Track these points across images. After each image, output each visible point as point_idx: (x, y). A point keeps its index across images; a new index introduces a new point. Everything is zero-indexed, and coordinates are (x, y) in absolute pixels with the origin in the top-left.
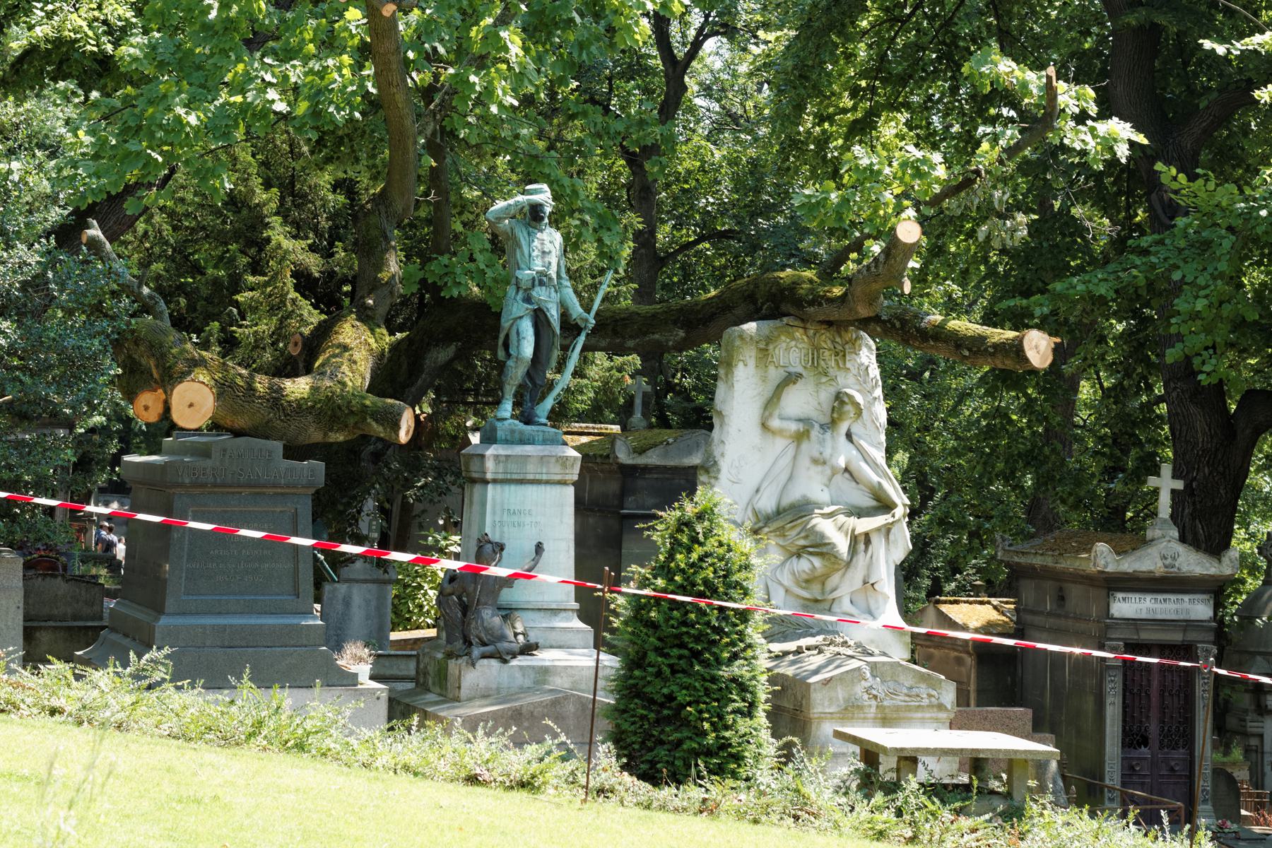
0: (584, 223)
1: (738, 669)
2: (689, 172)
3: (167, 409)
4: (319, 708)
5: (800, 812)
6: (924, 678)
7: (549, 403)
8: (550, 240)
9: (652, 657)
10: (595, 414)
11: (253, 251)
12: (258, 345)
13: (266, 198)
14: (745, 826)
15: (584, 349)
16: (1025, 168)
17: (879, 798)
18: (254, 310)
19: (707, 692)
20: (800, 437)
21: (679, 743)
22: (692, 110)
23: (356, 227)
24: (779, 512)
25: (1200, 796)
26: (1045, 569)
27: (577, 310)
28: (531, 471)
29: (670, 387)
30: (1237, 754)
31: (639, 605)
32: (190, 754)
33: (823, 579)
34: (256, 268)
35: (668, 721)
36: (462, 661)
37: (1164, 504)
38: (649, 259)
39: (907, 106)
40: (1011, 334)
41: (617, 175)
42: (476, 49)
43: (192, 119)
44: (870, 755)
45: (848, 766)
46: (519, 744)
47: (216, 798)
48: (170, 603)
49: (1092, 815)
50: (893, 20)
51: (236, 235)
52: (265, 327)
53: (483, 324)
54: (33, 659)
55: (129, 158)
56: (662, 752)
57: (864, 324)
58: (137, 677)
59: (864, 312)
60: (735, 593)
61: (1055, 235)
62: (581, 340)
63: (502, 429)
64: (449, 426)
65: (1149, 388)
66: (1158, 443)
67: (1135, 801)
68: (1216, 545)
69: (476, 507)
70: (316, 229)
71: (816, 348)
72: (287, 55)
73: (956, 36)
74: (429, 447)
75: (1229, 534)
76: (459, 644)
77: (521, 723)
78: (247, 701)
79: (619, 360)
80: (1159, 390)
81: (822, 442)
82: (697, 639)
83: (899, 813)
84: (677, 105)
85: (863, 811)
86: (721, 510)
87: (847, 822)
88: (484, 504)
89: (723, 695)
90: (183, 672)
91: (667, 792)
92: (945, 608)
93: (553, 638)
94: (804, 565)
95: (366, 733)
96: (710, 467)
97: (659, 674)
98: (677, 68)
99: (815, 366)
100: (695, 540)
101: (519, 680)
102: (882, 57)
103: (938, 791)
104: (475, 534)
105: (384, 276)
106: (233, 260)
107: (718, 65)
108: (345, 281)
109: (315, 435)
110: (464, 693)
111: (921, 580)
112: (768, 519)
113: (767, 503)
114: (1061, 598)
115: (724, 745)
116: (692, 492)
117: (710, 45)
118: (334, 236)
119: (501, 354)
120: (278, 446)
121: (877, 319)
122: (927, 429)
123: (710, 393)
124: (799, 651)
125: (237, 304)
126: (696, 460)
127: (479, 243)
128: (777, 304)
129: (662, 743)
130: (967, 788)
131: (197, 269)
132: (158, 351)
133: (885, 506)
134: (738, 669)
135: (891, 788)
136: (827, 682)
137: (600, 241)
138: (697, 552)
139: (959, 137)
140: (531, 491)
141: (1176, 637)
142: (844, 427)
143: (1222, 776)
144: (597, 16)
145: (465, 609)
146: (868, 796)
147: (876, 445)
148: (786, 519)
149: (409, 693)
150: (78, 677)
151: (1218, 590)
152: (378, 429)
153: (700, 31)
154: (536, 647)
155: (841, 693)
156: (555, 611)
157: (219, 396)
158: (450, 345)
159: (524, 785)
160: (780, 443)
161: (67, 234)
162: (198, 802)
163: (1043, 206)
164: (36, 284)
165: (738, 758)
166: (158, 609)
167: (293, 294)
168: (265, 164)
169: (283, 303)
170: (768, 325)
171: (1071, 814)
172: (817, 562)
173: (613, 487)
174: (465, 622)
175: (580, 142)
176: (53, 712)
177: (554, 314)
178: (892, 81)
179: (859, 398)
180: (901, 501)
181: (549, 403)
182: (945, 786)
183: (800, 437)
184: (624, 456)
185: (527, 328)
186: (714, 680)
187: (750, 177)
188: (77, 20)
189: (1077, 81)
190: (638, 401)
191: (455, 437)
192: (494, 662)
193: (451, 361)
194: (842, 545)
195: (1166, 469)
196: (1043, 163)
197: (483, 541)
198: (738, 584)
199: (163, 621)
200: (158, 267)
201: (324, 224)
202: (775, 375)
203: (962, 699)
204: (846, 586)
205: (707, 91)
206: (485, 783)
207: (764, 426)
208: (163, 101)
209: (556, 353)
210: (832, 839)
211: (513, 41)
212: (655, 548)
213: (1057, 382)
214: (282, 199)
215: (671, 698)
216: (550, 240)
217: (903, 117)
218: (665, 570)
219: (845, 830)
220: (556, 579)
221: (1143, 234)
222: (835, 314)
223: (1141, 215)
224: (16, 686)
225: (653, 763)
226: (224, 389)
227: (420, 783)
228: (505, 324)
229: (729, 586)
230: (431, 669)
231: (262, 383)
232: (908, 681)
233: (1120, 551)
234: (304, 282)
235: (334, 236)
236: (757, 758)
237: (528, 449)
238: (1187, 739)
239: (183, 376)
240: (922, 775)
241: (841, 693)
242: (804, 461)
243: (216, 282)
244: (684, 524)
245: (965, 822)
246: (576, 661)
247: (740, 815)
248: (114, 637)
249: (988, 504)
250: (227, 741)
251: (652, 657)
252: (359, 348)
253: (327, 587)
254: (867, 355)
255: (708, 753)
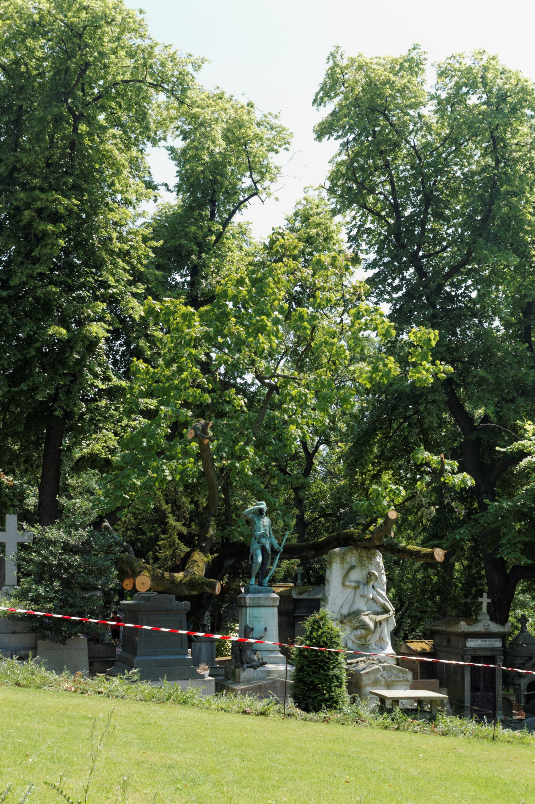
0: (278, 514)
1: (336, 671)
2: (315, 493)
3: (134, 585)
4: (191, 688)
5: (358, 719)
6: (401, 671)
7: (268, 578)
8: (266, 521)
9: (306, 668)
10: (284, 580)
11: (163, 526)
12: (166, 559)
13: (165, 507)
14: (340, 726)
15: (280, 559)
16: (434, 489)
17: (385, 715)
18: (164, 547)
19: (325, 679)
20: (356, 588)
21: (316, 697)
22: (316, 471)
23: (199, 517)
24: (349, 614)
25: (498, 708)
26: (443, 631)
27: (276, 546)
28: (262, 602)
29: (311, 569)
30: (511, 691)
31: (301, 651)
32: (146, 707)
33: (365, 637)
34: (164, 532)
35: (312, 690)
36: (241, 669)
37: (485, 606)
38: (302, 524)
39: (392, 468)
40: (429, 550)
41: (290, 495)
42: (238, 454)
43: (139, 483)
44: (383, 699)
45: (375, 704)
46: (261, 698)
47: (156, 723)
48: (139, 652)
49: (460, 718)
50: (386, 438)
51: (156, 521)
52: (168, 553)
53: (243, 551)
54: (92, 673)
55: (117, 498)
56: (310, 701)
57: (378, 547)
58: (127, 679)
59: (377, 543)
60: (334, 645)
61: (445, 510)
62: (278, 556)
63: (251, 588)
64: (234, 586)
65: (480, 565)
66: (483, 585)
67: (476, 711)
68: (502, 620)
69: (243, 616)
70: (184, 518)
71: (361, 557)
72: (170, 458)
73: (409, 443)
74: (227, 593)
75: (508, 616)
76: (239, 663)
77: (261, 691)
78: (166, 686)
79: (292, 561)
80: (483, 565)
81: (364, 590)
82: (322, 661)
83: (393, 720)
84: (310, 469)
85: (380, 719)
86: (329, 616)
87: (375, 723)
88: (246, 615)
89: (331, 681)
90: (144, 677)
91: (312, 715)
92: (408, 644)
93: (272, 660)
94: (359, 632)
95: (208, 697)
96: (325, 599)
97: (308, 674)
98: (310, 456)
99: (361, 563)
100: (319, 627)
101: (260, 675)
102: (382, 452)
103: (407, 712)
104: (244, 625)
105: (208, 536)
106: (156, 530)
107: (325, 454)
108: (195, 535)
109: (187, 593)
110: (241, 680)
111: (399, 636)
112: (346, 617)
113: (345, 611)
114: (449, 641)
115: (332, 698)
116: (318, 611)
117: (322, 447)
118: (191, 520)
119: (250, 562)
120: (173, 597)
121: (382, 546)
122: (401, 581)
123: (325, 571)
124: (357, 662)
125: (158, 545)
126: (320, 596)
127: (241, 521)
128: (347, 541)
129: (309, 697)
130: (416, 710)
131: (144, 533)
132: (130, 564)
133: (386, 611)
134: (336, 671)
135: (390, 711)
136: (367, 673)
137: (284, 520)
138: (321, 631)
139: (411, 479)
140: (263, 610)
141: (489, 653)
142: (371, 584)
143: (506, 700)
144: (280, 440)
145: (241, 651)
146: (382, 714)
147: (383, 590)
148: (352, 617)
149: (223, 680)
150: (107, 680)
151: (503, 636)
152: (208, 590)
153: (318, 442)
154: (266, 663)
155: (372, 677)
156: (272, 651)
157: (152, 580)
158: (232, 558)
159: (263, 714)
160: (349, 590)
161: (97, 524)
162: (150, 724)
163: (441, 503)
164: (87, 543)
165: (336, 702)
166: (135, 654)
167: (178, 541)
168: (166, 495)
169: (174, 544)
170: (343, 549)
171: (453, 718)
172: (363, 631)
173: (291, 606)
174: (241, 656)
175: (276, 486)
176: (99, 693)
177: (268, 547)
178: (386, 459)
179: (376, 574)
180: (392, 609)
181: (268, 578)
182: (409, 710)
183: (356, 588)
184: (295, 596)
185: (259, 552)
186: (328, 675)
187: (337, 494)
188: (98, 447)
189: (452, 458)
190: (299, 576)
191: (236, 590)
192: (252, 669)
193: (233, 564)
194: (372, 625)
195: (485, 595)
196: (440, 490)
197: (246, 627)
198: (335, 643)
199: (137, 658)
200: (130, 533)
201: (187, 516)
202: (347, 566)
203: (415, 677)
204: (373, 640)
205: (321, 463)
206: (249, 714)
207: (343, 584)
208: (128, 477)
209: (270, 561)
210: (370, 729)
211: (250, 449)
212: (305, 630)
213: (447, 565)
214: (172, 508)
215: (313, 682)
216: (266, 521)
217: (391, 472)
218: (309, 638)
219: (375, 726)
220: (272, 641)
221: (477, 513)
222: (367, 545)
223: (476, 505)
224: (86, 684)
225: (307, 705)
226: (154, 578)
227: (227, 714)
228: (251, 551)
229: (332, 643)
230: (230, 672)
231: (167, 575)
232: (395, 672)
233: (469, 624)
234: (181, 536)
235: (191, 520)
236: (343, 702)
237: (261, 595)
238: (493, 688)
239: (139, 573)
240: (401, 706)
241: (372, 677)
242: (358, 596)
243: (151, 538)
244: (315, 622)
245: (416, 722)
246: (279, 668)
247: (338, 722)
248: (120, 664)
249: (422, 608)
250: (160, 701)
251: (306, 668)
252: (200, 562)
253: (193, 644)
254: (379, 559)
255: (327, 700)
